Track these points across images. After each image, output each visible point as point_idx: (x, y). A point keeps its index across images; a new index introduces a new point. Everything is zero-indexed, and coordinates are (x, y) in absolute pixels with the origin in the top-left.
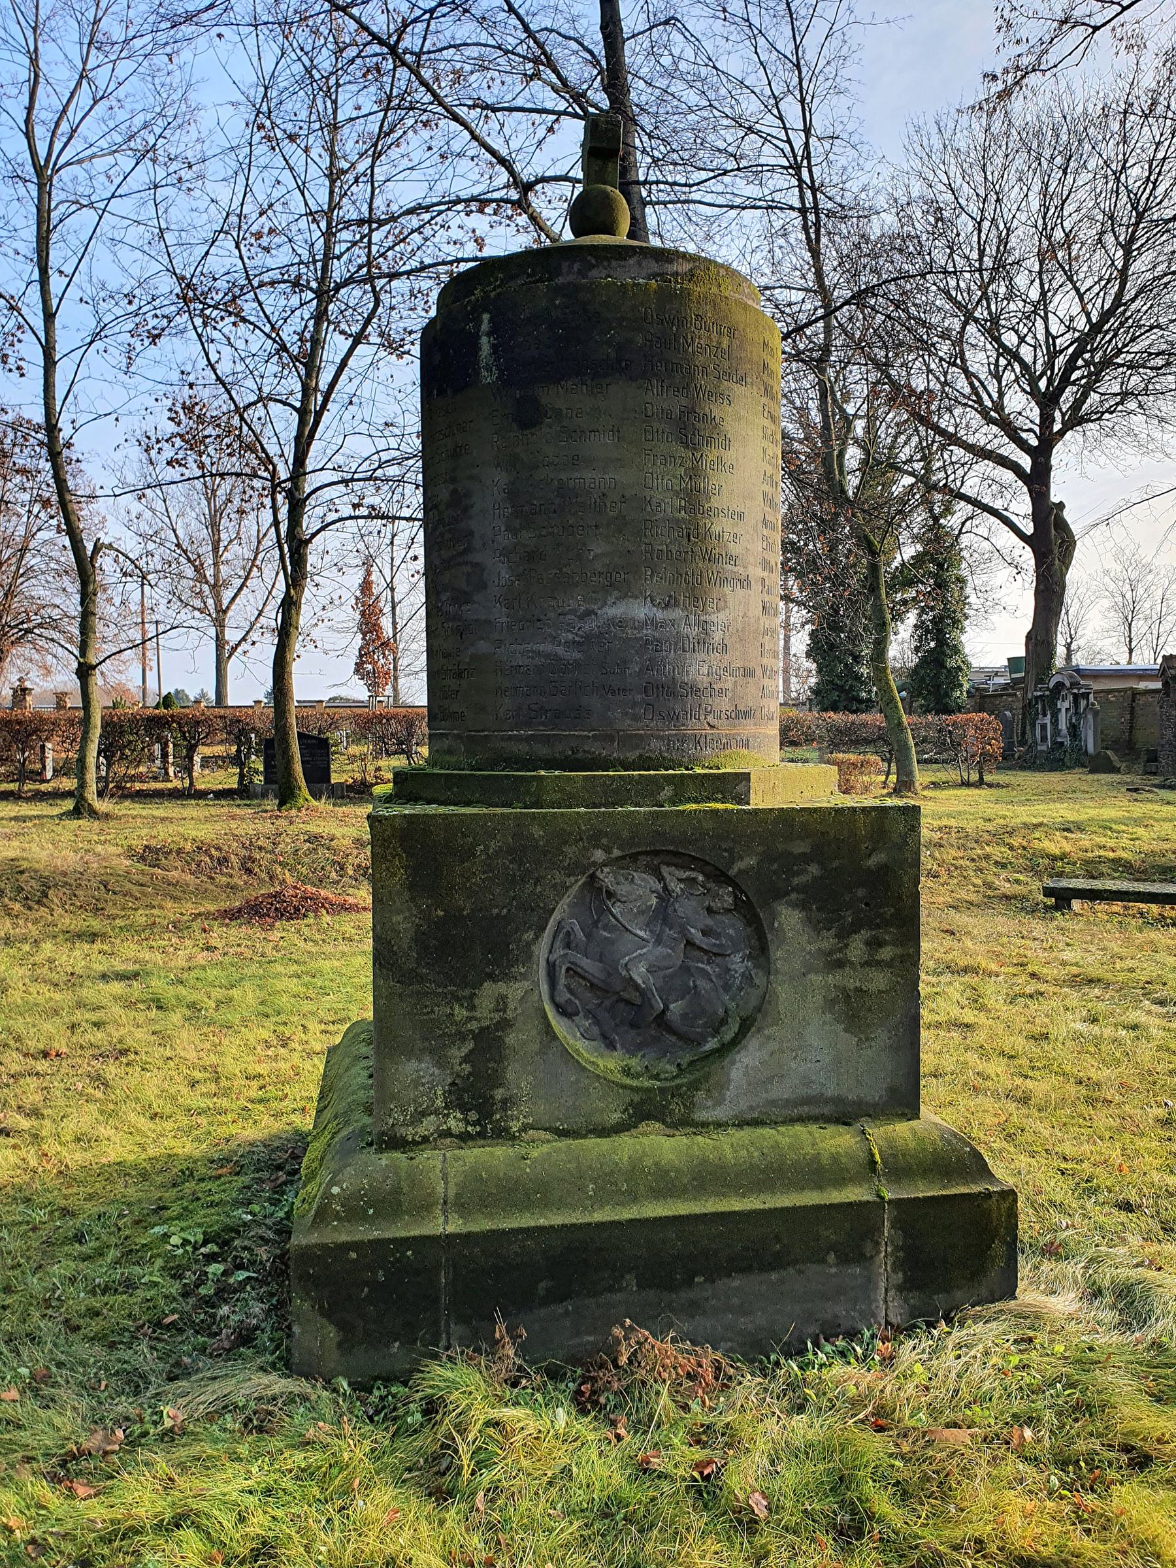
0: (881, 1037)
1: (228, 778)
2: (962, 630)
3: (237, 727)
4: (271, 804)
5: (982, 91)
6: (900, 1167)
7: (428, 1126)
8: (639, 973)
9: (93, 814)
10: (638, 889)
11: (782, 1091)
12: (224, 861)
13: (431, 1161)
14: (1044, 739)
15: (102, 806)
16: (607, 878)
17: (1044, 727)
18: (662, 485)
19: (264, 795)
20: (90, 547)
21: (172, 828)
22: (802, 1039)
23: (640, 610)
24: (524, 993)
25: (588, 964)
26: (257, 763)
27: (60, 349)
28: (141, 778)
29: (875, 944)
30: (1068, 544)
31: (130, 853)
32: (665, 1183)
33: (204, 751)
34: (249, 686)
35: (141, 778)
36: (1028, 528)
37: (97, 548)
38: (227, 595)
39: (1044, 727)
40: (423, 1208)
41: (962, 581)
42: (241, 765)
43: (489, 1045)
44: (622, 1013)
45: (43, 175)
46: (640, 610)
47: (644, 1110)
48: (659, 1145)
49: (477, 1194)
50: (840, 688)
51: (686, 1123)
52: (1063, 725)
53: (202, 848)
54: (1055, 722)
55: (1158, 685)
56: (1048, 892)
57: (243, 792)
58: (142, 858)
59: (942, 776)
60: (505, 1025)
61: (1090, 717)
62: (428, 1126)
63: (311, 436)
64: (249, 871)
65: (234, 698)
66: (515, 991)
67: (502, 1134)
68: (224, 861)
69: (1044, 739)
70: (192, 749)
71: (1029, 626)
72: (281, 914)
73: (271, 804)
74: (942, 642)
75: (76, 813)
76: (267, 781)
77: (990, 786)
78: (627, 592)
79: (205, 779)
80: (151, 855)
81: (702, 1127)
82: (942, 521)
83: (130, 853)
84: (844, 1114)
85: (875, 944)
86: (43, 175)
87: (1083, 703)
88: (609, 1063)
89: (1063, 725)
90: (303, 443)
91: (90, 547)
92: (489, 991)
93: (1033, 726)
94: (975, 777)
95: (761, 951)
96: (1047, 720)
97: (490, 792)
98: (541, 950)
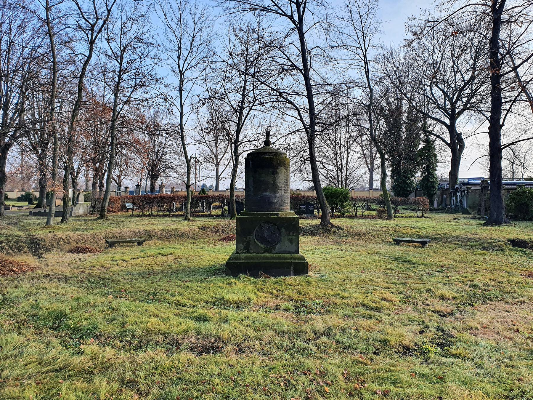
0: (294, 244)
1: (219, 212)
2: (436, 170)
3: (221, 199)
4: (229, 218)
5: (405, 43)
6: (295, 259)
7: (241, 251)
8: (266, 236)
9: (189, 220)
10: (266, 226)
11: (283, 250)
12: (218, 230)
13: (242, 255)
14: (454, 204)
15: (191, 218)
16: (262, 224)
17: (453, 200)
18: (271, 180)
19: (227, 217)
20: (189, 158)
21: (207, 223)
22: (285, 245)
23: (268, 194)
24: (253, 237)
25: (260, 235)
26: (226, 208)
27: (184, 112)
28: (198, 211)
29: (293, 233)
30: (462, 146)
31: (199, 228)
32: (267, 258)
33: (214, 204)
34: (224, 185)
35: (198, 211)
36: (449, 142)
37: (191, 157)
38: (219, 157)
39: (453, 200)
40: (241, 259)
41: (435, 155)
42: (223, 209)
43: (248, 243)
44: (263, 240)
45: (181, 73)
46: (268, 194)
47: (266, 251)
48: (267, 255)
49: (245, 258)
50: (401, 187)
51: (270, 253)
52: (459, 200)
53: (214, 227)
54: (457, 199)
55: (480, 188)
56: (394, 240)
57: (223, 216)
58: (201, 229)
59: (412, 214)
60: (250, 240)
61: (465, 197)
62: (241, 251)
63: (240, 130)
64: (223, 232)
65: (221, 188)
66: (251, 237)
67: (250, 253)
68: (218, 230)
69: (454, 204)
70: (211, 204)
71: (450, 170)
72: (229, 240)
73: (229, 218)
74: (429, 173)
75: (185, 219)
76: (229, 213)
77: (425, 217)
78: (266, 192)
79: (215, 212)
80: (203, 228)
81: (273, 253)
82: (429, 137)
83: (199, 228)
84: (290, 253)
85: (293, 233)
86: (181, 73)
87: (463, 194)
88: (262, 246)
89: (459, 200)
90: (238, 131)
91: (189, 158)
92: (248, 237)
93: (451, 200)
94: (421, 215)
95: (280, 234)
96: (454, 198)
97: (251, 215)
98: (254, 232)
